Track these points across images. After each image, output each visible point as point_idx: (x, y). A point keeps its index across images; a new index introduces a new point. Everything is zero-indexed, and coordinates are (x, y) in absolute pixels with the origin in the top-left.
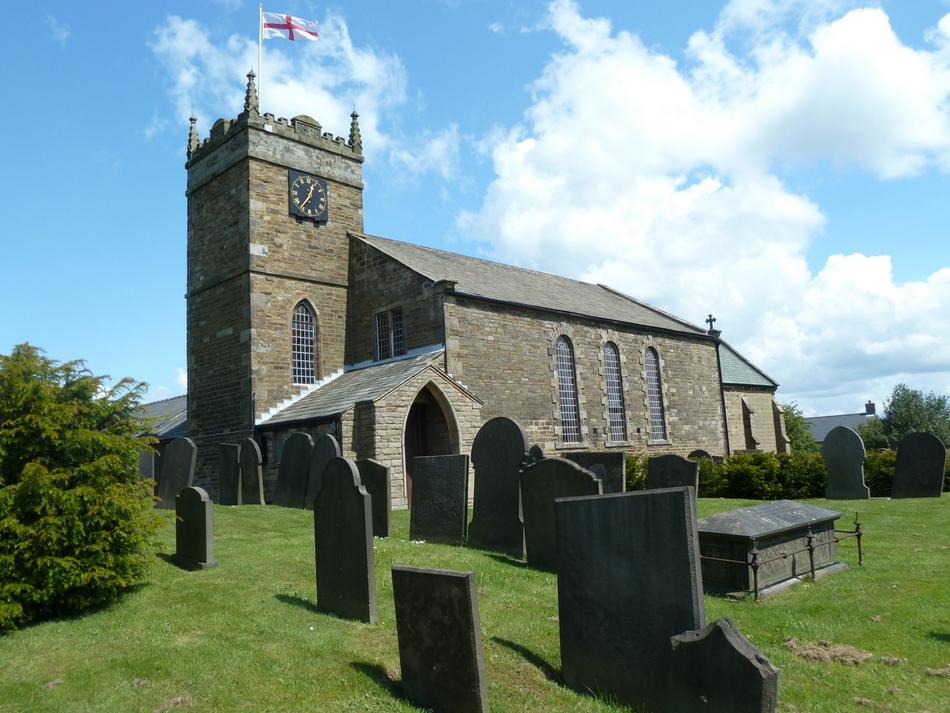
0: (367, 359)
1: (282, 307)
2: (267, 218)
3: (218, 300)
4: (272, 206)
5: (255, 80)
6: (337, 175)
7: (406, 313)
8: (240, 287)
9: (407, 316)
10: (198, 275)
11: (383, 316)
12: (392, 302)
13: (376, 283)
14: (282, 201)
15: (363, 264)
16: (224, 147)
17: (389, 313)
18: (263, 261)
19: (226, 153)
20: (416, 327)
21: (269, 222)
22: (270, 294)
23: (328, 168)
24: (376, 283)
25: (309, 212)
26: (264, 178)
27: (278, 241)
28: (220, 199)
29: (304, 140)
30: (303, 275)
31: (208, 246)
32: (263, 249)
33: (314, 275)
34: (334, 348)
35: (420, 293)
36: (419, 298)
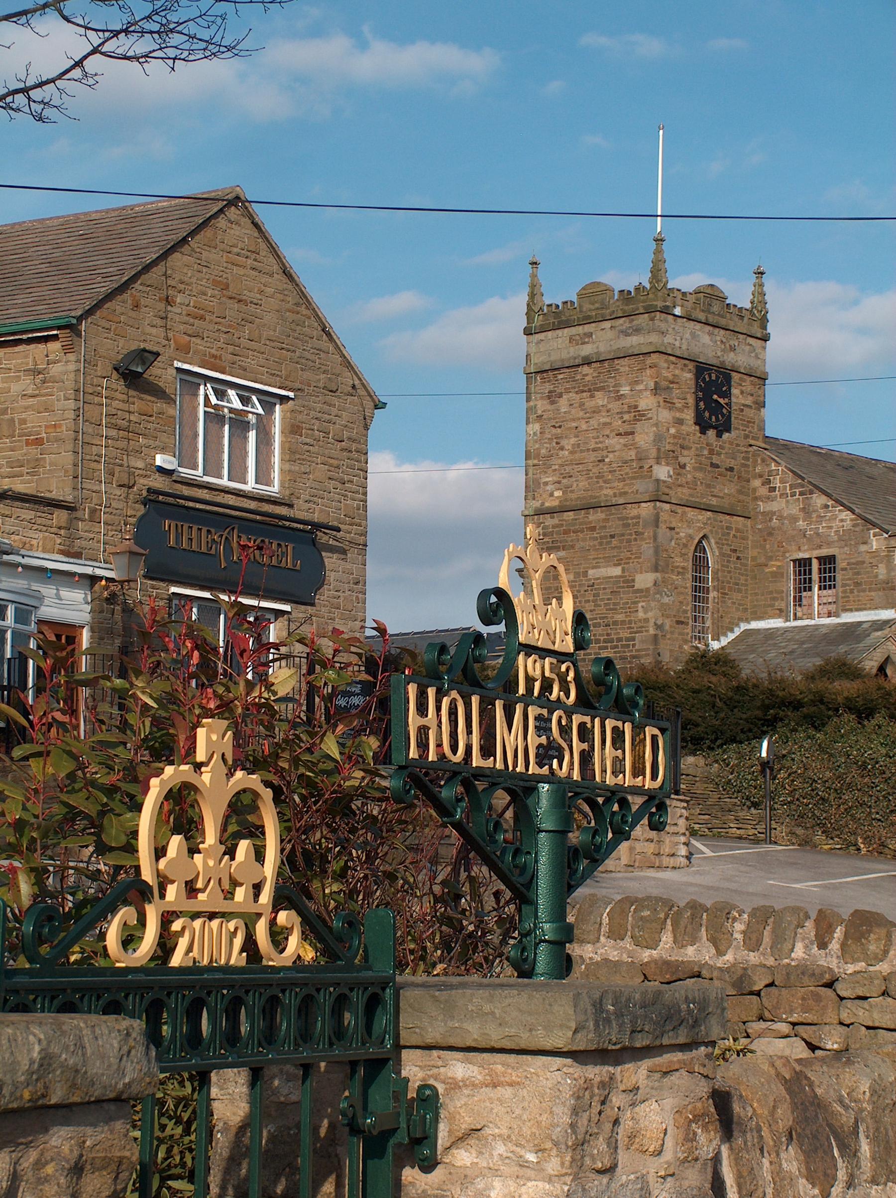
0: (772, 617)
1: (685, 546)
2: (672, 431)
3: (593, 529)
4: (678, 415)
5: (665, 246)
6: (740, 363)
7: (841, 564)
8: (638, 517)
9: (843, 569)
10: (549, 488)
11: (803, 565)
12: (820, 547)
13: (794, 519)
14: (686, 406)
15: (773, 489)
16: (607, 325)
17: (815, 563)
18: (668, 487)
19: (610, 334)
20: (857, 584)
21: (674, 437)
22: (674, 529)
23: (732, 355)
24: (794, 519)
25: (714, 418)
26: (671, 378)
27: (682, 460)
28: (598, 394)
29: (711, 320)
30: (704, 504)
31: (571, 453)
32: (669, 472)
33: (715, 503)
34: (40, 549)
35: (865, 543)
36: (863, 548)
